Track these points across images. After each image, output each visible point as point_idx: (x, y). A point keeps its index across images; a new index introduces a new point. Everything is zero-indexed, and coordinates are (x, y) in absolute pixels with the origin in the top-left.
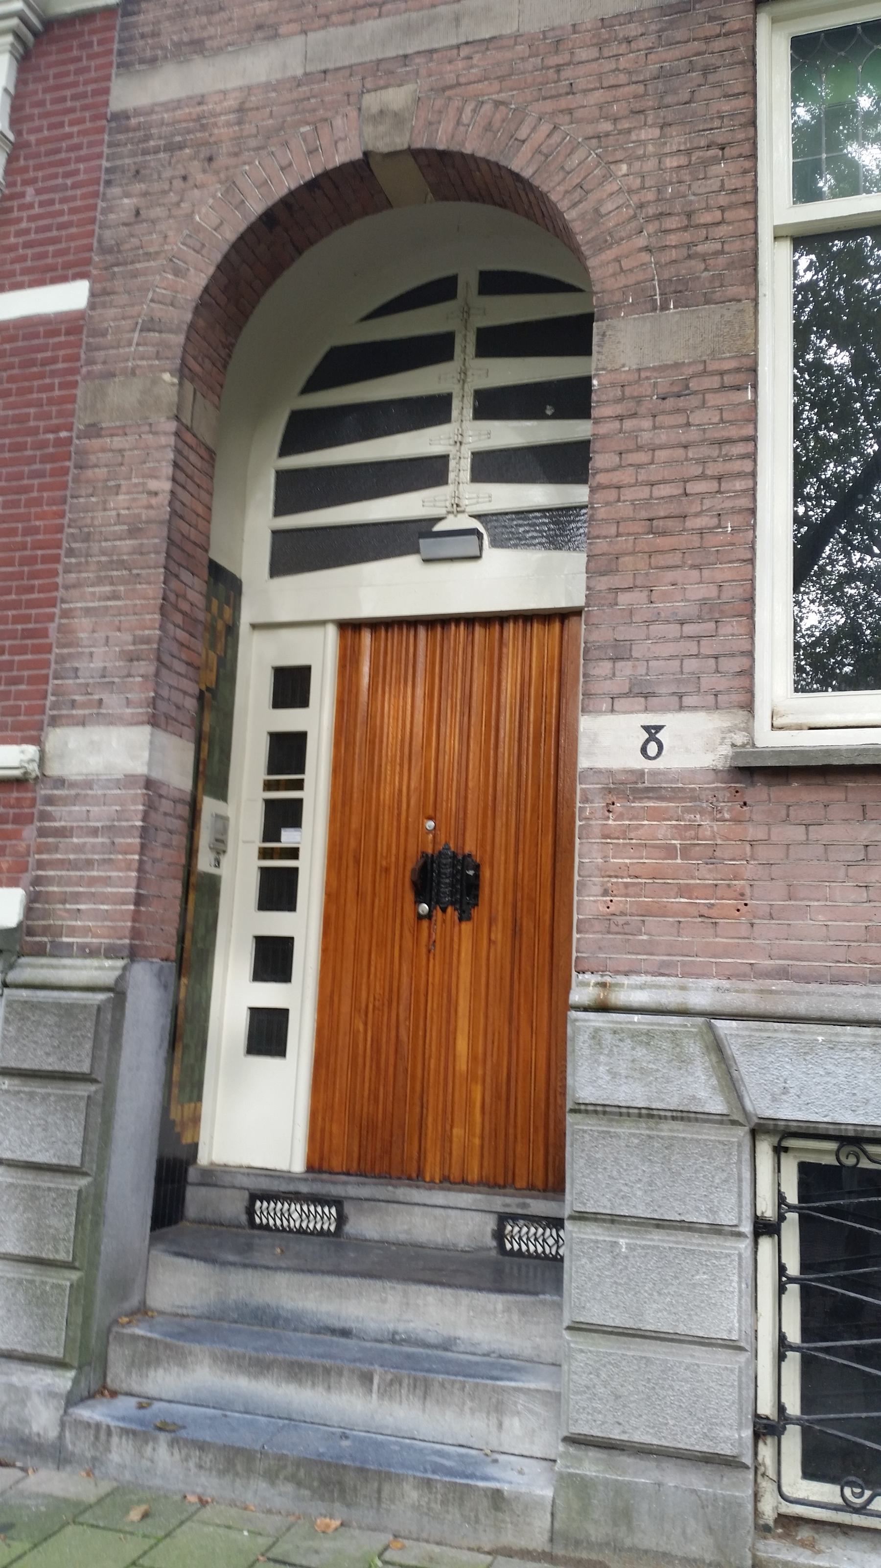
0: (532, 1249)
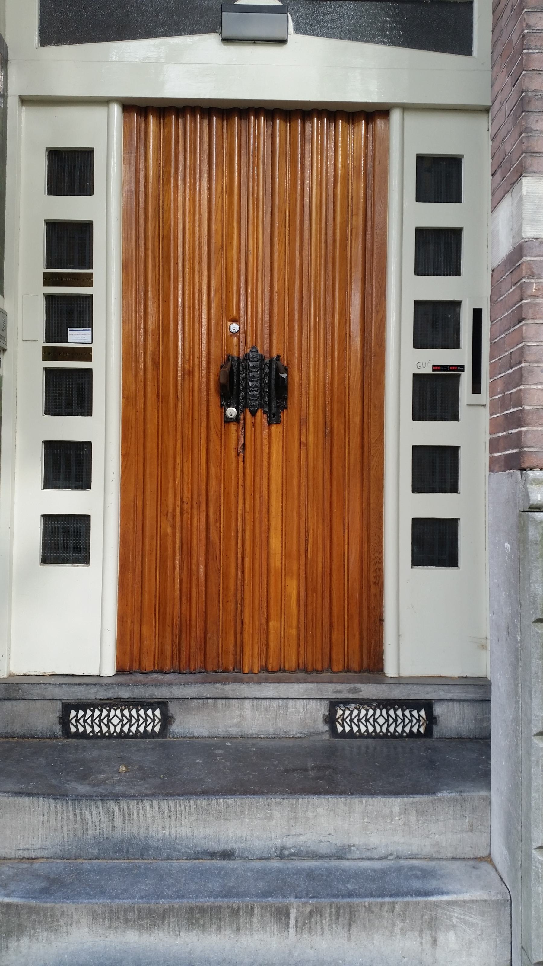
0: (363, 729)
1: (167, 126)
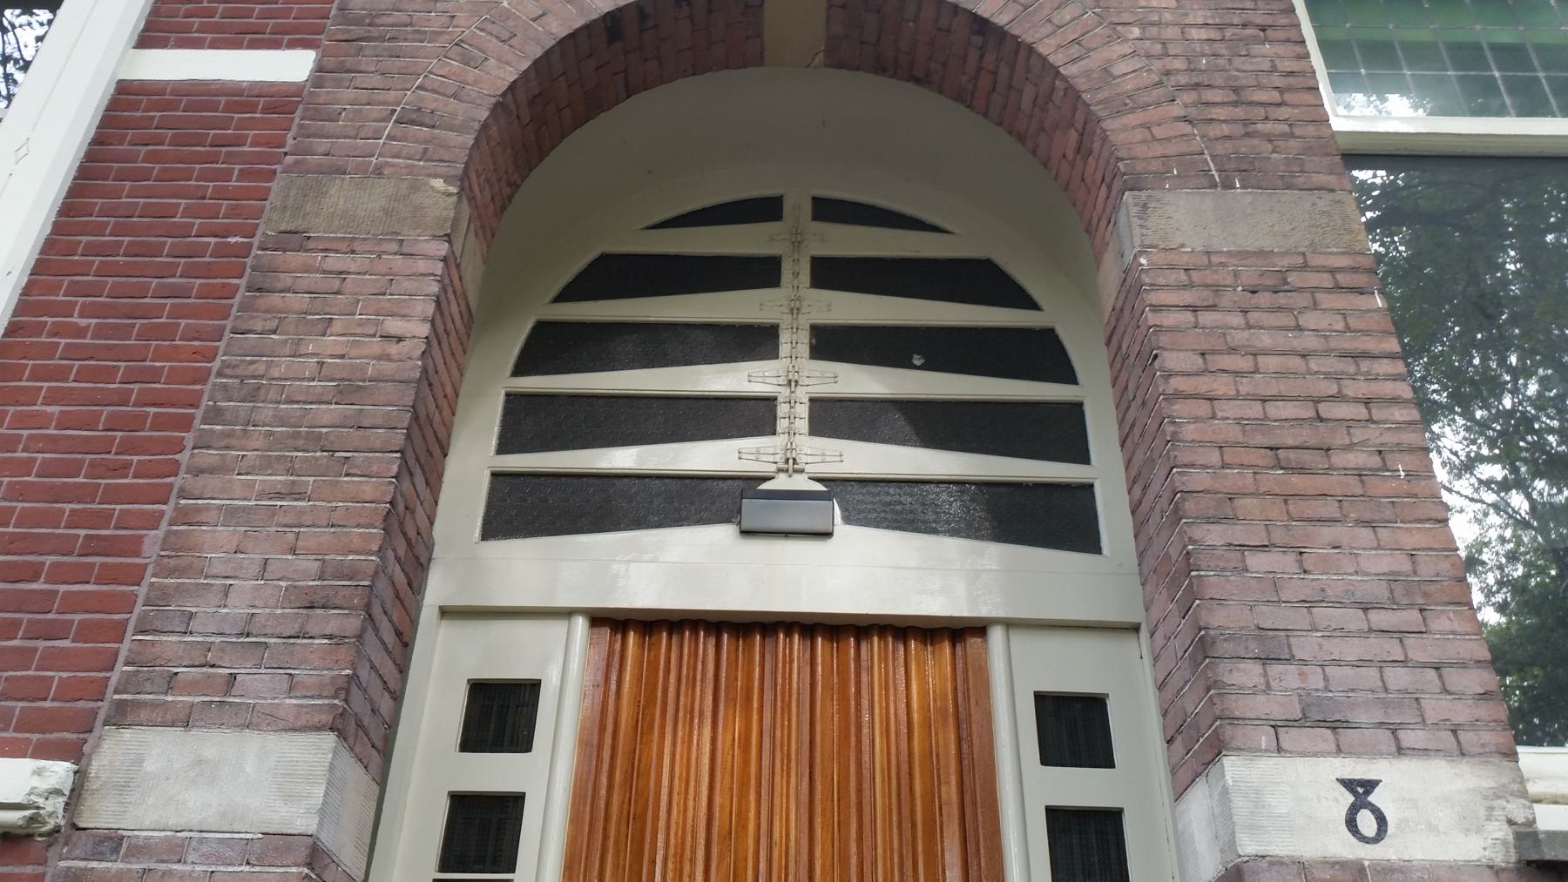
1: (654, 647)
